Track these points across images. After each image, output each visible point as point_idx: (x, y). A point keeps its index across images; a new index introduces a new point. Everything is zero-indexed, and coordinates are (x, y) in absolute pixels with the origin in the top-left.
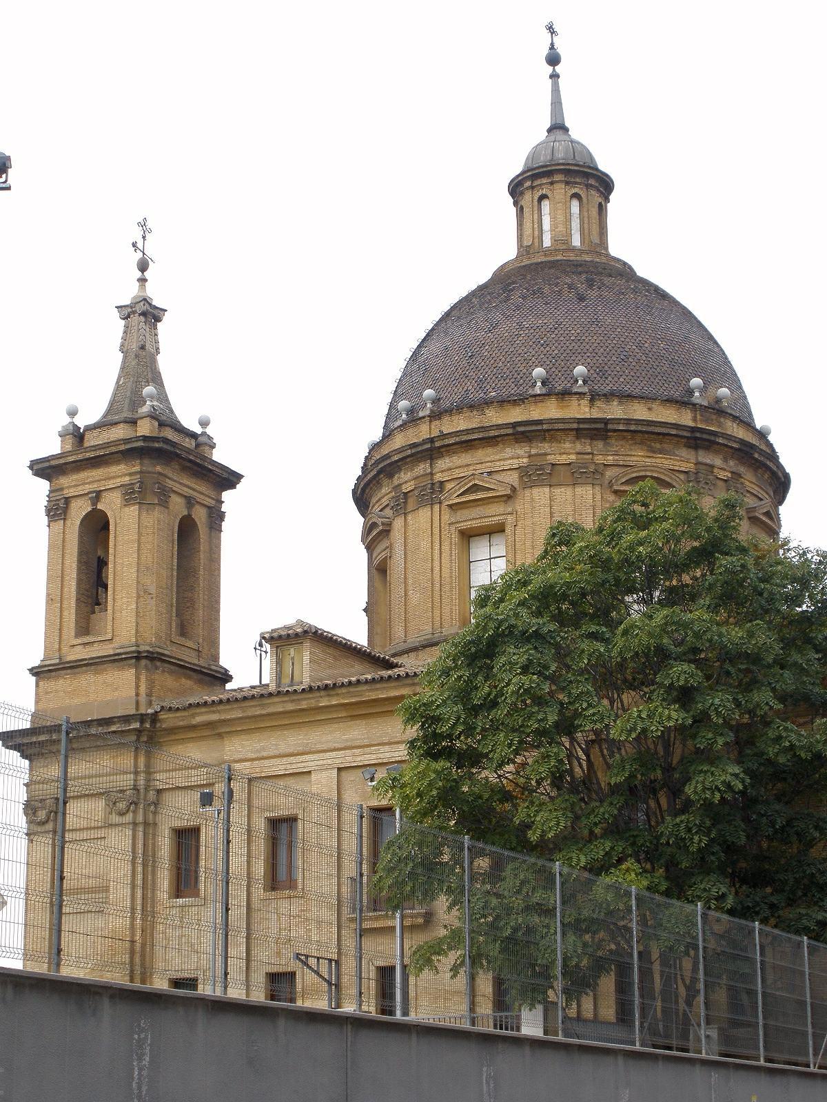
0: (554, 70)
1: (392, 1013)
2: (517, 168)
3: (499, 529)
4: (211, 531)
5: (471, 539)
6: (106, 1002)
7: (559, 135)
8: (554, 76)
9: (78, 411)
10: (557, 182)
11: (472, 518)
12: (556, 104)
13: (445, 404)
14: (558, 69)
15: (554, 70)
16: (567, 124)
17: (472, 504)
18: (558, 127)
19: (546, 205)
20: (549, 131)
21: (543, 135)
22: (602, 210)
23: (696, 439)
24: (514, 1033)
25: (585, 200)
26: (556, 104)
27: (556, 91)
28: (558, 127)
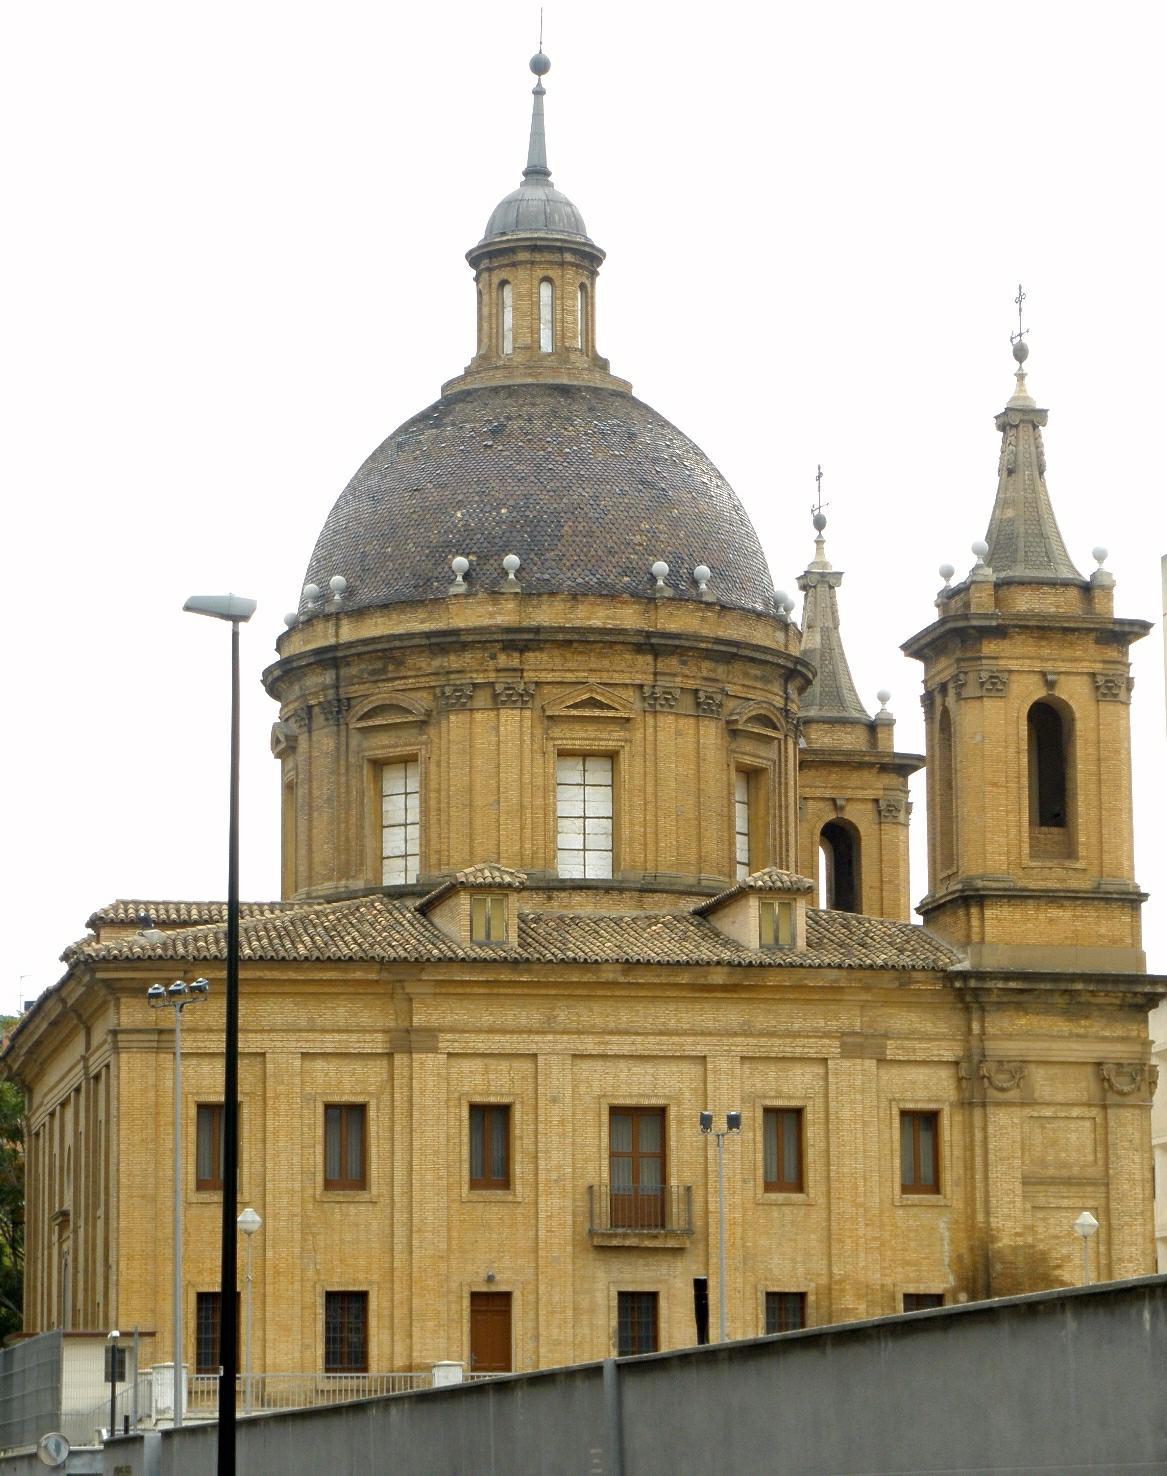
1: (214, 1340)
3: (407, 761)
4: (1098, 705)
5: (409, 764)
6: (271, 1423)
9: (253, 610)
10: (521, 263)
11: (382, 745)
14: (546, 80)
18: (537, 173)
19: (508, 291)
22: (587, 291)
24: (651, 1355)
25: (558, 282)
27: (538, 115)
28: (537, 173)
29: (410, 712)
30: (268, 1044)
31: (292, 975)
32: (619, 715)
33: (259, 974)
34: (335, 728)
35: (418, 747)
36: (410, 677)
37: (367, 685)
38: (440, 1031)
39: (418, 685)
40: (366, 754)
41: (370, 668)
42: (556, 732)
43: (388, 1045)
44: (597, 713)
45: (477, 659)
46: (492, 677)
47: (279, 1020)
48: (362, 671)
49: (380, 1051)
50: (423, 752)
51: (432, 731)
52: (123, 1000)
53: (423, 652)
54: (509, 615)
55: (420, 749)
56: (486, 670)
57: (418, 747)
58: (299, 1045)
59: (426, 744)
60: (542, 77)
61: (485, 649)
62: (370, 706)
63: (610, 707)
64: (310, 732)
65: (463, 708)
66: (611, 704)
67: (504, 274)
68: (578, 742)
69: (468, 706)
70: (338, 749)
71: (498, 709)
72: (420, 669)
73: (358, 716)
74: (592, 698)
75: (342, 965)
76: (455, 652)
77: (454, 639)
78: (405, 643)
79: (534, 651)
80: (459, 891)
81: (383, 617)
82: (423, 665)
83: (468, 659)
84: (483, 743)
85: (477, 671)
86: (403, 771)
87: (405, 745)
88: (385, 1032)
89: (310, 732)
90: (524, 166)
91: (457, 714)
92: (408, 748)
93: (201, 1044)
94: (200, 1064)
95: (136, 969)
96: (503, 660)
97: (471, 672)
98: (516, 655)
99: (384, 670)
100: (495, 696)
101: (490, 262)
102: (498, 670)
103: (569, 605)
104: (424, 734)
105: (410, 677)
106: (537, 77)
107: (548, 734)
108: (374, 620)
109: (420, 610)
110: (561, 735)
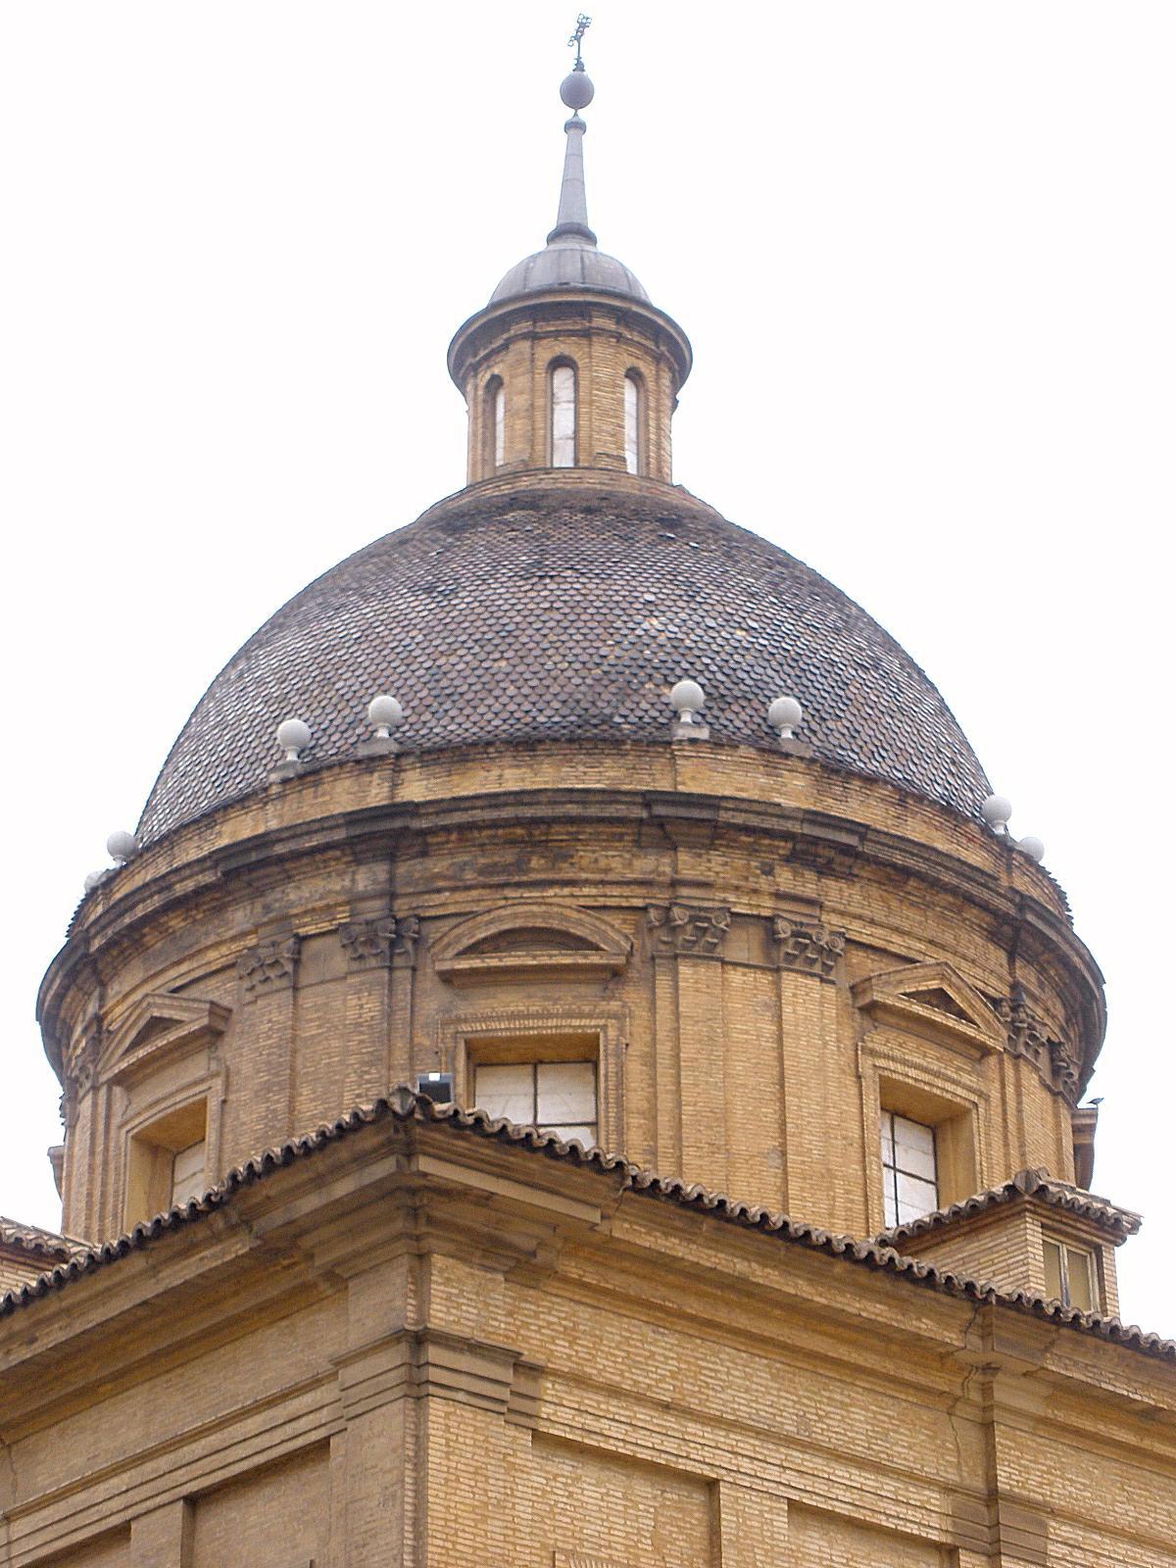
0: (576, 115)
2: (477, 299)
5: (540, 1068)
7: (571, 244)
8: (575, 127)
10: (601, 332)
12: (573, 184)
13: (327, 752)
14: (584, 114)
15: (576, 115)
16: (593, 226)
17: (958, 1045)
18: (572, 230)
20: (553, 237)
21: (541, 245)
23: (660, 822)
26: (573, 184)
27: (574, 157)
28: (572, 230)
29: (598, 948)
30: (725, 1458)
31: (799, 1287)
32: (971, 1032)
33: (741, 1267)
34: (385, 974)
35: (602, 1022)
36: (586, 882)
37: (474, 893)
38: (1053, 1513)
39: (601, 901)
40: (465, 1028)
41: (482, 861)
42: (877, 1040)
43: (947, 1525)
44: (951, 1021)
45: (735, 869)
46: (766, 906)
47: (741, 1407)
48: (462, 867)
49: (934, 1536)
50: (612, 1033)
51: (633, 996)
52: (438, 1260)
53: (620, 837)
54: (798, 799)
55: (604, 1027)
56: (755, 891)
57: (602, 1022)
58: (784, 1478)
59: (615, 1016)
60: (580, 111)
61: (752, 851)
62: (493, 930)
63: (961, 1015)
64: (296, 989)
65: (710, 956)
66: (970, 1012)
67: (562, 348)
68: (912, 1072)
69: (719, 952)
70: (389, 1015)
71: (778, 970)
72: (607, 870)
73: (461, 947)
74: (942, 990)
75: (905, 1288)
76: (691, 847)
77: (706, 814)
78: (593, 811)
79: (838, 877)
80: (1020, 1214)
81: (518, 767)
82: (616, 864)
83: (714, 865)
84: (747, 1032)
85: (737, 888)
86: (530, 1080)
87: (569, 1015)
88: (947, 1489)
89: (296, 989)
90: (551, 225)
91: (695, 965)
92: (576, 1022)
93: (591, 1423)
94: (578, 1479)
95: (503, 1173)
96: (785, 879)
97: (725, 888)
98: (810, 875)
99: (520, 866)
100: (772, 940)
101: (534, 325)
102: (779, 896)
103: (892, 811)
104: (612, 998)
105: (586, 882)
106: (573, 111)
107: (863, 1041)
108: (496, 772)
109: (608, 762)
110: (885, 1049)
